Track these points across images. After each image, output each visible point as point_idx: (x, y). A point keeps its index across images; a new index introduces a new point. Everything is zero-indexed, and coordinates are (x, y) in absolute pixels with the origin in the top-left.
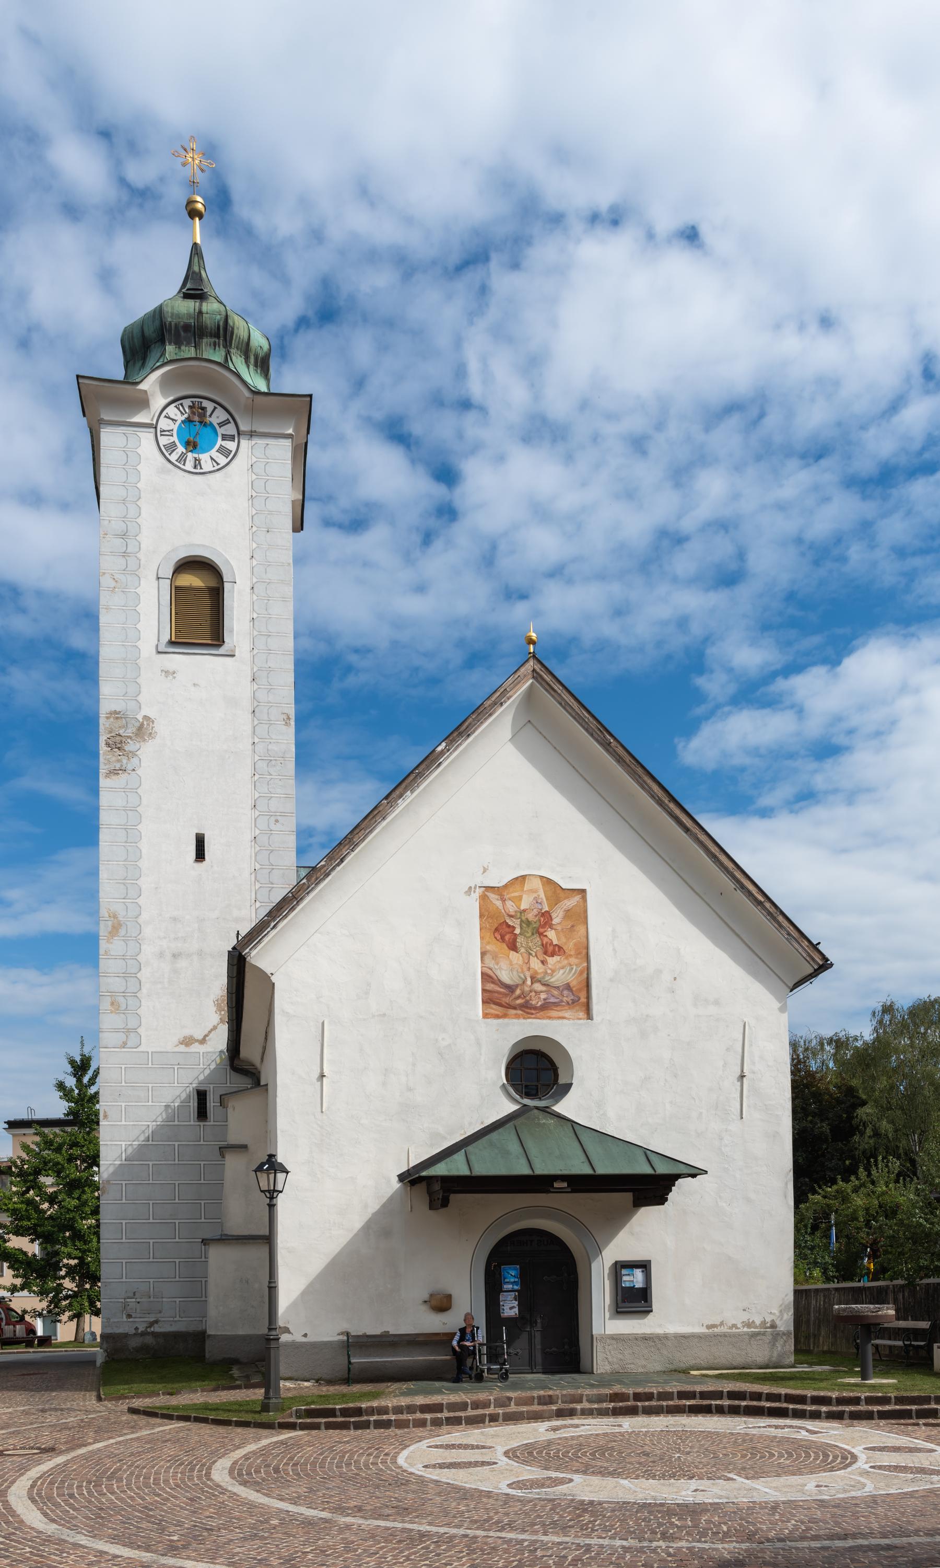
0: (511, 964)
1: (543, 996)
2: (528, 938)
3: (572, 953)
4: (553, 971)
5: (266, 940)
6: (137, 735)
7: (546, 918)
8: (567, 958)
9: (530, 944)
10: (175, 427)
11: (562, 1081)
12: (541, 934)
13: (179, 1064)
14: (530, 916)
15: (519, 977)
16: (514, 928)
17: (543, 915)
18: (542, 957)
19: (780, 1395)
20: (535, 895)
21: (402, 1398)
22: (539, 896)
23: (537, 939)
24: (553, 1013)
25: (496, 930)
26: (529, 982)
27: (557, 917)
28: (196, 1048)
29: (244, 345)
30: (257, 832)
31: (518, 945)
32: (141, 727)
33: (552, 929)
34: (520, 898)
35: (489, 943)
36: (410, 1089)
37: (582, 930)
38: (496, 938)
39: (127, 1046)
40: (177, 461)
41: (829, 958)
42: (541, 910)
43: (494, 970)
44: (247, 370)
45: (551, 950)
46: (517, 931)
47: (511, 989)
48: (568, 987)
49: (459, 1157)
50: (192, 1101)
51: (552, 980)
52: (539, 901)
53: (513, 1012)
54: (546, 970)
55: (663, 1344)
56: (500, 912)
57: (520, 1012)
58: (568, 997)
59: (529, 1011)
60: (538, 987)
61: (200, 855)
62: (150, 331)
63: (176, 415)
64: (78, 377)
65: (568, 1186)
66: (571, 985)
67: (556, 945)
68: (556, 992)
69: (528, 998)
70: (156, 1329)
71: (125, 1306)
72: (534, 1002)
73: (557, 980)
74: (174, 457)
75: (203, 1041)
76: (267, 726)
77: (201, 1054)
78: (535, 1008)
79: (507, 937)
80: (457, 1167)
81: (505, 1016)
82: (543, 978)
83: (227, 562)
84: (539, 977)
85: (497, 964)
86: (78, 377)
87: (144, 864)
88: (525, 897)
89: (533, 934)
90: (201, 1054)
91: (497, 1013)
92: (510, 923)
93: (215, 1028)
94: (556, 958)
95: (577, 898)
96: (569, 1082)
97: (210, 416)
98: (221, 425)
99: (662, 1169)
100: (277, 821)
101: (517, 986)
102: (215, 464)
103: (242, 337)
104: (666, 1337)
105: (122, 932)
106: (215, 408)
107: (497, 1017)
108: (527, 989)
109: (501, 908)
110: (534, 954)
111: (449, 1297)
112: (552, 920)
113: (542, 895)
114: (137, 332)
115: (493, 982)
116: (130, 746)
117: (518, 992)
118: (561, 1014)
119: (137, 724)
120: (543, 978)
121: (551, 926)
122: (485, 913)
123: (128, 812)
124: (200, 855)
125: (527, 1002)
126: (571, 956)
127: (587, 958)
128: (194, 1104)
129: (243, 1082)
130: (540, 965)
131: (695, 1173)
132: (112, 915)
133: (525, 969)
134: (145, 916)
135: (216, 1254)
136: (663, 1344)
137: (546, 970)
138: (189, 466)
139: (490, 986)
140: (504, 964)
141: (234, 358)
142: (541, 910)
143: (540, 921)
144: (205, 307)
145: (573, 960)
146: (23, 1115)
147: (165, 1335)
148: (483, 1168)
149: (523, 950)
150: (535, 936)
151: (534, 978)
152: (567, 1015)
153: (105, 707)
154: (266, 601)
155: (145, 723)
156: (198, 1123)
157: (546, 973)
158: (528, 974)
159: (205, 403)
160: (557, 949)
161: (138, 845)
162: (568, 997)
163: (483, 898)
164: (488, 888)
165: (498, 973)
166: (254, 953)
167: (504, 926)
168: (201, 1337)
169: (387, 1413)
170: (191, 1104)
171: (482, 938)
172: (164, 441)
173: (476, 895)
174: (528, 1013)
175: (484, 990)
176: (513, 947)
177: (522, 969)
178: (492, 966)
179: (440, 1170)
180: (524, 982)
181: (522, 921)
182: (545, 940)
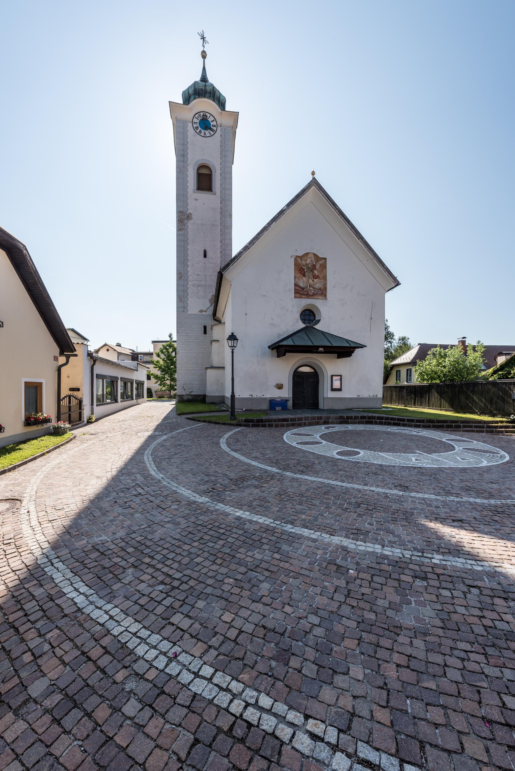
1: (313, 291)
5: (229, 269)
10: (198, 121)
11: (317, 319)
12: (313, 272)
14: (310, 266)
18: (313, 279)
19: (375, 417)
24: (316, 297)
28: (204, 313)
32: (188, 216)
36: (272, 319)
45: (315, 277)
46: (306, 270)
47: (303, 289)
48: (320, 289)
49: (290, 339)
53: (303, 296)
58: (320, 292)
60: (311, 288)
61: (205, 256)
68: (316, 290)
70: (192, 394)
71: (183, 387)
74: (198, 131)
75: (205, 311)
78: (310, 295)
80: (289, 342)
81: (301, 298)
83: (213, 165)
87: (189, 258)
93: (209, 308)
94: (317, 280)
95: (324, 260)
99: (353, 345)
104: (345, 398)
105: (183, 278)
107: (299, 298)
111: (282, 385)
114: (187, 92)
116: (185, 222)
121: (316, 269)
122: (296, 264)
124: (205, 256)
127: (326, 280)
129: (216, 323)
131: (362, 346)
134: (189, 273)
135: (209, 371)
138: (202, 134)
139: (297, 288)
140: (301, 281)
145: (322, 280)
146: (156, 340)
147: (195, 396)
148: (298, 343)
159: (207, 114)
162: (320, 292)
163: (295, 259)
164: (297, 256)
166: (226, 273)
168: (204, 396)
169: (271, 422)
171: (295, 272)
172: (195, 126)
173: (293, 259)
175: (295, 289)
176: (304, 275)
179: (285, 343)
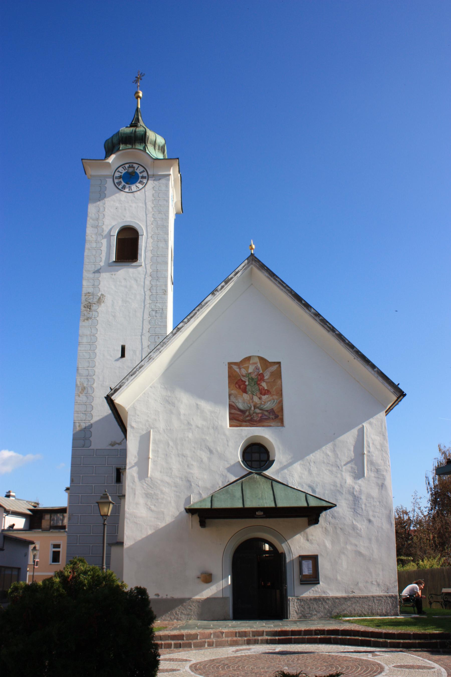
0: (244, 400)
2: (252, 386)
3: (275, 393)
4: (265, 403)
6: (98, 302)
7: (261, 377)
8: (272, 396)
9: (253, 390)
12: (259, 385)
13: (108, 455)
14: (253, 376)
15: (248, 406)
16: (245, 382)
17: (259, 375)
20: (255, 365)
21: (363, 627)
22: (257, 366)
23: (257, 387)
25: (237, 383)
26: (253, 408)
27: (267, 376)
29: (154, 142)
30: (149, 343)
31: (247, 390)
32: (100, 298)
33: (264, 382)
34: (248, 367)
35: (233, 390)
37: (279, 382)
38: (236, 387)
39: (85, 446)
40: (122, 188)
41: (404, 391)
42: (259, 372)
43: (235, 403)
44: (154, 151)
46: (247, 383)
47: (243, 412)
50: (114, 473)
51: (265, 407)
52: (258, 368)
53: (244, 424)
54: (261, 402)
55: (326, 602)
56: (239, 375)
57: (248, 424)
59: (252, 423)
62: (115, 140)
63: (122, 170)
64: (82, 159)
65: (264, 514)
66: (274, 409)
67: (266, 390)
69: (252, 416)
72: (255, 419)
73: (266, 408)
74: (120, 187)
76: (156, 295)
77: (119, 450)
78: (256, 421)
79: (242, 386)
81: (240, 426)
82: (260, 406)
84: (258, 405)
85: (237, 400)
86: (82, 159)
88: (250, 366)
89: (255, 384)
90: (119, 450)
91: (237, 424)
92: (243, 379)
94: (266, 396)
96: (274, 459)
97: (136, 170)
98: (141, 173)
99: (313, 503)
100: (159, 338)
101: (247, 410)
102: (137, 188)
103: (152, 139)
105: (85, 392)
106: (139, 167)
108: (252, 412)
109: (239, 372)
110: (255, 394)
112: (264, 377)
113: (259, 365)
115: (235, 409)
116: (94, 307)
117: (247, 413)
118: (269, 424)
119: (98, 298)
120: (260, 406)
121: (264, 380)
123: (92, 337)
125: (252, 418)
126: (274, 395)
127: (281, 395)
128: (114, 475)
130: (258, 400)
132: (81, 384)
133: (251, 401)
136: (326, 602)
137: (261, 402)
139: (233, 411)
141: (149, 147)
142: (259, 372)
143: (258, 378)
144: (138, 129)
145: (275, 397)
149: (249, 393)
150: (256, 385)
151: (255, 406)
152: (272, 425)
153: (84, 291)
154: (157, 242)
155: (101, 297)
156: (116, 485)
157: (261, 404)
158: (252, 405)
160: (267, 392)
161: (95, 351)
165: (237, 404)
167: (240, 381)
170: (113, 475)
171: (229, 387)
174: (252, 424)
176: (245, 391)
177: (249, 402)
178: (234, 401)
180: (250, 408)
181: (249, 378)
182: (261, 387)
